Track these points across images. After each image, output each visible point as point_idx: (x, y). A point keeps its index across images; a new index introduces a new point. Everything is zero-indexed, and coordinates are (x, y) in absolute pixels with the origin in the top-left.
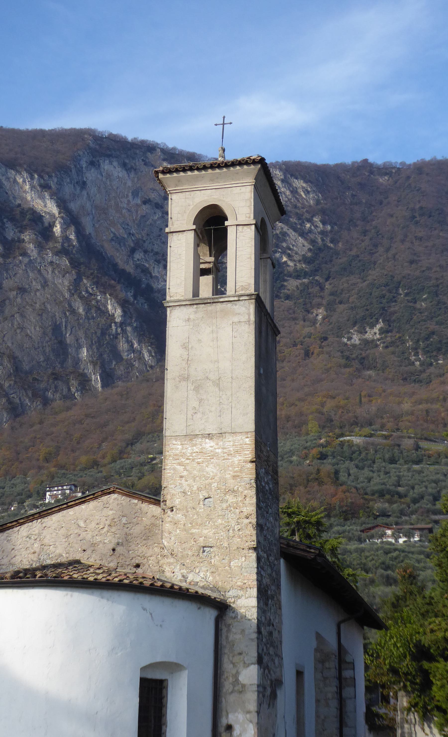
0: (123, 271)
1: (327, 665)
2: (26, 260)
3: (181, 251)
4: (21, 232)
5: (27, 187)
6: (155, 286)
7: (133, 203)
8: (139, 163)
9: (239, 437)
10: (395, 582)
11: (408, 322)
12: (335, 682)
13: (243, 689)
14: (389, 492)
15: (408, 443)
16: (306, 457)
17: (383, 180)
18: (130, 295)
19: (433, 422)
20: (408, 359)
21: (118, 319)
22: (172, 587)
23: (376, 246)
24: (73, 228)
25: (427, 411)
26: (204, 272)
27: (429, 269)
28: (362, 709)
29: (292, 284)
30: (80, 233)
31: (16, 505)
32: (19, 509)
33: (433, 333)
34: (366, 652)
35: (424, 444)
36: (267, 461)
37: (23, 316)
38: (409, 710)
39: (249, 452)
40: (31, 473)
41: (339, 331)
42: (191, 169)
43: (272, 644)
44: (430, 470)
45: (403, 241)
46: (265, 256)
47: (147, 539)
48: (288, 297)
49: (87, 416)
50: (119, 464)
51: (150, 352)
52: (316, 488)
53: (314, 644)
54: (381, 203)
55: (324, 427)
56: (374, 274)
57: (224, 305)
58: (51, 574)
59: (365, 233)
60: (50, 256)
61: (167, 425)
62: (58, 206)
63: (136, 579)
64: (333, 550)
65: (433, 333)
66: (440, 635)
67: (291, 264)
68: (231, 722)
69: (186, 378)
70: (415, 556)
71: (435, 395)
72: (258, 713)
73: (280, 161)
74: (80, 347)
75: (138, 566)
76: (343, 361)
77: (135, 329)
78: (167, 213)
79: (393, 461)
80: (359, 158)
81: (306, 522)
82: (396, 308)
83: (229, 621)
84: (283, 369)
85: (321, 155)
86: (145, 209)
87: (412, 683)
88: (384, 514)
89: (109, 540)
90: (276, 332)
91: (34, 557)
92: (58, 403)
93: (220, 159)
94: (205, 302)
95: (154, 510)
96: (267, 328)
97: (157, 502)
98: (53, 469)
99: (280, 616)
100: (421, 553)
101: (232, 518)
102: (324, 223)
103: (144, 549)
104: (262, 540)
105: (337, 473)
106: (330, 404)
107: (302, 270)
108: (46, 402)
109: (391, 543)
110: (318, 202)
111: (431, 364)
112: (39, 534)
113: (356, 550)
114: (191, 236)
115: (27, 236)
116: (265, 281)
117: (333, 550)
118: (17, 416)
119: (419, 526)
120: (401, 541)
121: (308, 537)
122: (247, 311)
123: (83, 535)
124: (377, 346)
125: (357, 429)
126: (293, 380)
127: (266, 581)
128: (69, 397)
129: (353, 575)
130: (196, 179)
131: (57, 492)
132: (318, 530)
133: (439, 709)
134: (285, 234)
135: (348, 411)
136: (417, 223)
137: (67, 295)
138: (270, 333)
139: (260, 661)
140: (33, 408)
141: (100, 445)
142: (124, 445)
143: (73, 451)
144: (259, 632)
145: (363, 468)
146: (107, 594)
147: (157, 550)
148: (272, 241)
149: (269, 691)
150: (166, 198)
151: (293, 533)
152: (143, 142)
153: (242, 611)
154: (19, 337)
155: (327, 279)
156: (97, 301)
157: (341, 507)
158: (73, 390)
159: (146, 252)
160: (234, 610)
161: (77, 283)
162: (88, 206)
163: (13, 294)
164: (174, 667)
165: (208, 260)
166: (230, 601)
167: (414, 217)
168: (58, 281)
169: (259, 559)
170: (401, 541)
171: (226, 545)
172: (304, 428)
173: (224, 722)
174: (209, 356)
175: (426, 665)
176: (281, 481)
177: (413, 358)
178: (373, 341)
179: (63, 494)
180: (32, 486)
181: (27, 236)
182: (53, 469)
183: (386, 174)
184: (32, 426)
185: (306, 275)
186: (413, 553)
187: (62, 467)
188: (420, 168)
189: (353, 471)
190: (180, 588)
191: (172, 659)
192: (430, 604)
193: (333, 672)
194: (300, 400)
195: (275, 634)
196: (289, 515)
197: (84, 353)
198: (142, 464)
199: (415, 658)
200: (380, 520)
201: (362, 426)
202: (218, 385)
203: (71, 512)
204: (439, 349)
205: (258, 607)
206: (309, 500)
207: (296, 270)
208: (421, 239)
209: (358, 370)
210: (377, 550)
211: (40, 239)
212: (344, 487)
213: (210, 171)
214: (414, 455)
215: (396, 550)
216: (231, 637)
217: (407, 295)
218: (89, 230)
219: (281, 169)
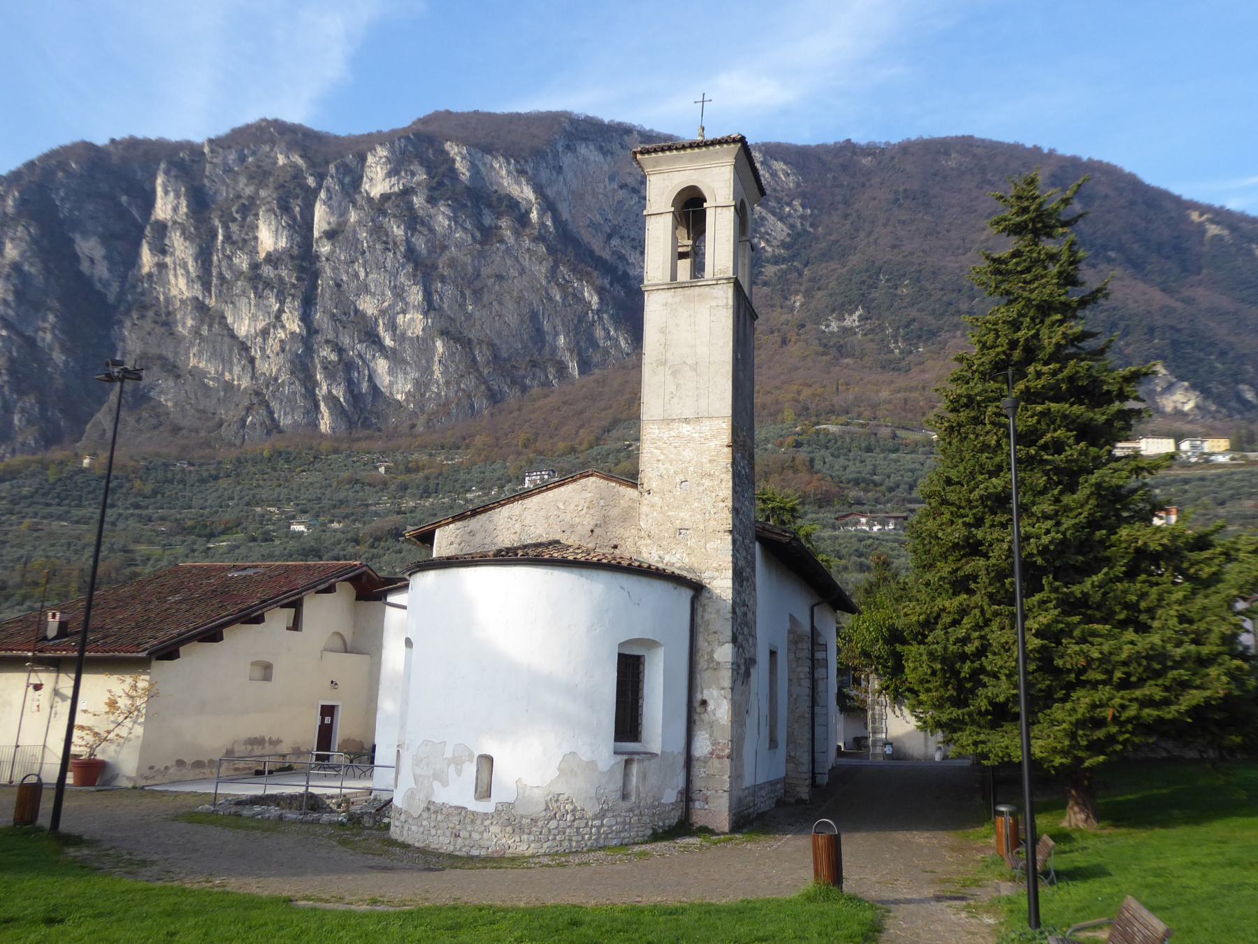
0: (600, 257)
1: (800, 646)
2: (503, 247)
3: (660, 234)
4: (498, 218)
5: (504, 172)
6: (631, 273)
7: (609, 187)
8: (615, 147)
9: (716, 422)
10: (869, 569)
11: (888, 308)
12: (809, 663)
13: (717, 666)
14: (864, 480)
15: (885, 432)
16: (781, 445)
17: (866, 161)
18: (606, 282)
19: (911, 411)
20: (887, 347)
21: (595, 307)
22: (649, 567)
23: (857, 230)
24: (549, 214)
25: (905, 400)
26: (682, 256)
27: (911, 253)
28: (833, 690)
29: (770, 270)
30: (557, 220)
31: (496, 489)
32: (499, 493)
33: (914, 320)
34: (838, 635)
35: (900, 433)
36: (744, 446)
37: (500, 303)
38: (880, 692)
39: (726, 437)
40: (511, 458)
41: (818, 318)
42: (670, 149)
43: (746, 624)
44: (907, 459)
45: (885, 225)
46: (744, 238)
47: (625, 520)
48: (765, 284)
49: (564, 403)
50: (594, 451)
51: (626, 339)
52: (791, 475)
53: (788, 626)
54: (863, 185)
55: (799, 415)
56: (854, 259)
57: (702, 289)
58: (532, 553)
59: (846, 216)
60: (527, 243)
61: (644, 409)
62: (535, 192)
63: (614, 559)
64: (808, 536)
65: (914, 320)
66: (914, 618)
67: (769, 249)
68: (705, 697)
69: (664, 363)
70: (890, 544)
71: (914, 384)
72: (732, 689)
73: (759, 142)
74: (557, 334)
75: (615, 547)
76: (821, 349)
77: (612, 317)
78: (645, 198)
79: (869, 449)
80: (842, 139)
81: (780, 508)
82: (877, 295)
83: (705, 601)
84: (760, 357)
85: (803, 135)
86: (622, 194)
87: (884, 666)
88: (859, 502)
89: (588, 522)
90: (754, 316)
91: (516, 538)
92: (536, 390)
93: (700, 138)
94: (683, 286)
95: (631, 493)
96: (745, 313)
97: (635, 486)
98: (532, 455)
99: (755, 597)
100: (894, 541)
101: (708, 501)
102: (804, 207)
103: (622, 531)
104: (737, 523)
105: (812, 461)
106: (806, 392)
107: (780, 255)
108: (524, 389)
109: (865, 531)
110: (798, 185)
111: (911, 352)
112: (520, 515)
113: (830, 537)
114: (670, 217)
115: (504, 223)
116: (744, 265)
117: (808, 536)
118: (496, 402)
119: (894, 514)
120: (875, 529)
121: (783, 523)
122: (726, 294)
123: (563, 516)
124: (855, 333)
125: (833, 418)
126: (769, 368)
127: (741, 563)
128: (547, 384)
129: (827, 561)
130: (675, 159)
131: (536, 477)
132: (793, 516)
133: (910, 690)
134: (763, 219)
135: (825, 400)
136: (900, 206)
137: (544, 283)
138: (748, 317)
139: (734, 640)
140: (512, 395)
141: (577, 432)
142: (600, 431)
143: (551, 437)
144: (734, 612)
145: (838, 457)
146: (586, 572)
147: (634, 532)
148: (750, 225)
149: (743, 669)
150: (643, 182)
151: (768, 519)
152: (620, 124)
153: (718, 591)
154: (497, 325)
155: (806, 266)
156: (574, 289)
157: (815, 495)
158: (551, 377)
159: (622, 238)
160: (709, 591)
161: (554, 270)
162: (565, 191)
163: (490, 282)
164: (651, 644)
165: (686, 243)
166: (705, 582)
167: (897, 200)
168: (535, 268)
169: (734, 542)
170: (875, 529)
171: (702, 527)
172: (779, 417)
173: (699, 697)
174: (687, 340)
175: (899, 648)
176: (757, 469)
177: (892, 346)
178: (852, 328)
179: (542, 479)
180: (512, 472)
181: (504, 223)
182: (532, 455)
183: (869, 155)
184: (511, 412)
185: (784, 260)
186: (887, 541)
187: (541, 453)
188: (906, 149)
189: (829, 459)
190: (657, 569)
191: (649, 636)
192: (904, 589)
193: (806, 653)
194: (776, 388)
195: (750, 615)
196: (764, 501)
197: (562, 340)
198: (618, 451)
199: (887, 641)
200: (855, 508)
201: (838, 415)
202: (695, 370)
203: (550, 493)
204: (920, 337)
205: (733, 588)
206: (783, 488)
207: (774, 256)
208: (904, 222)
209: (836, 358)
210: (851, 537)
211: (517, 226)
212: (819, 475)
213: (689, 151)
214: (890, 444)
215: (870, 537)
216: (707, 616)
217: (888, 281)
218: (565, 216)
219: (760, 151)
